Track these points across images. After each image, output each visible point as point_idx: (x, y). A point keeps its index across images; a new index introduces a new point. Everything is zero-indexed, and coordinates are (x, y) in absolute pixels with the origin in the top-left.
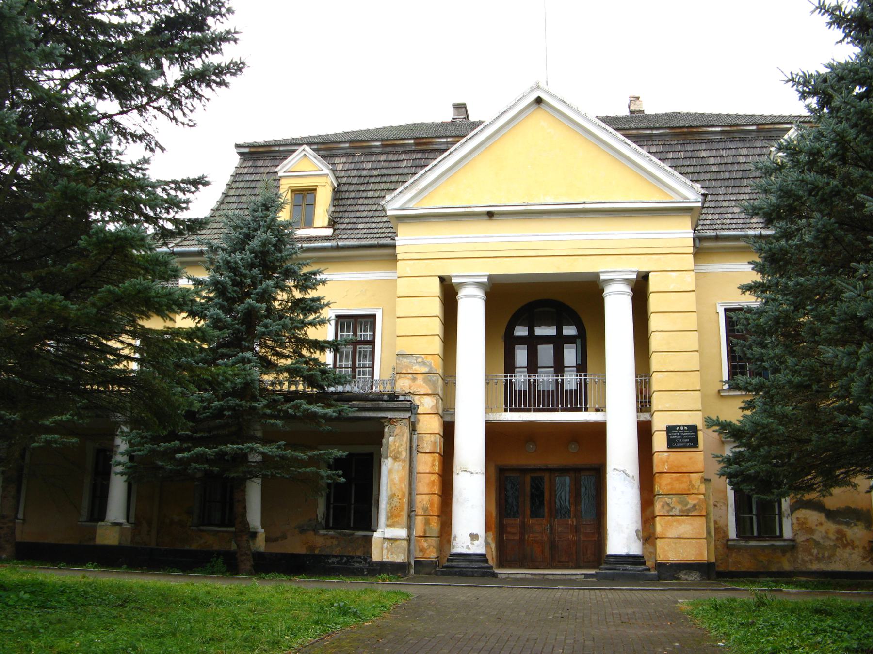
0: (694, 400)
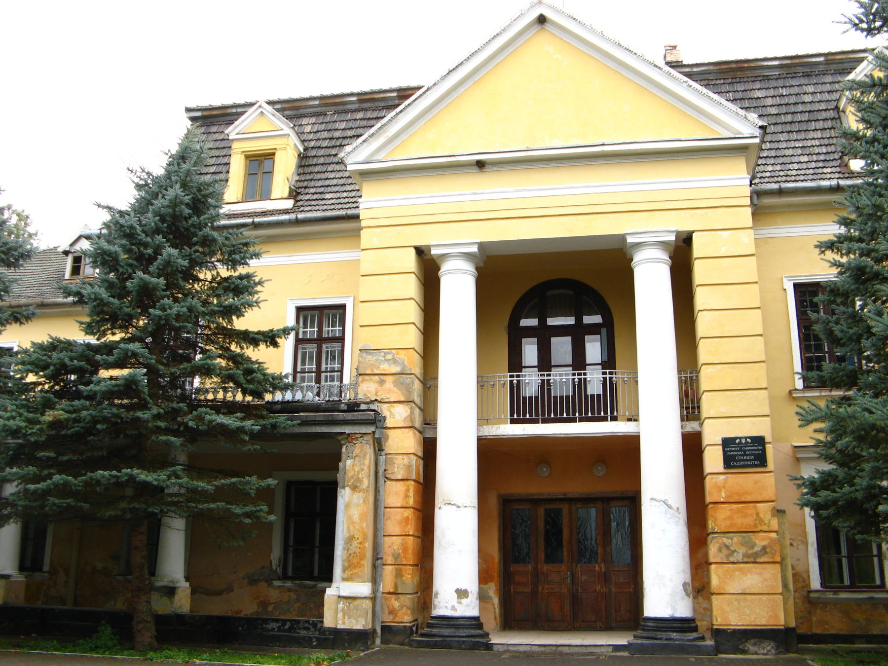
0: (759, 402)
